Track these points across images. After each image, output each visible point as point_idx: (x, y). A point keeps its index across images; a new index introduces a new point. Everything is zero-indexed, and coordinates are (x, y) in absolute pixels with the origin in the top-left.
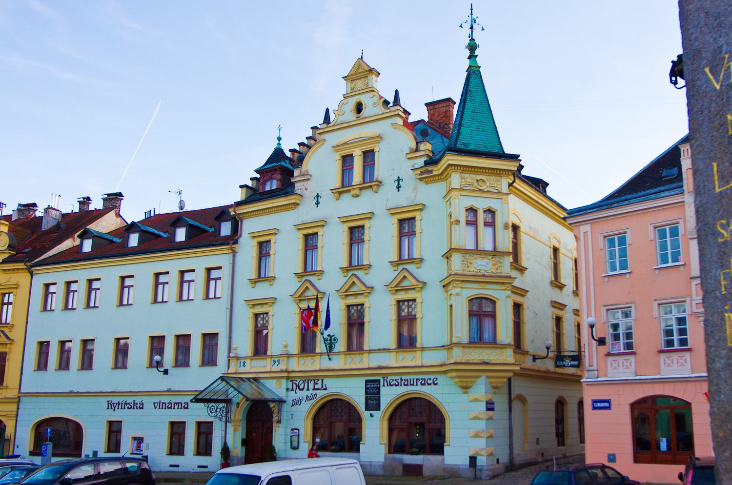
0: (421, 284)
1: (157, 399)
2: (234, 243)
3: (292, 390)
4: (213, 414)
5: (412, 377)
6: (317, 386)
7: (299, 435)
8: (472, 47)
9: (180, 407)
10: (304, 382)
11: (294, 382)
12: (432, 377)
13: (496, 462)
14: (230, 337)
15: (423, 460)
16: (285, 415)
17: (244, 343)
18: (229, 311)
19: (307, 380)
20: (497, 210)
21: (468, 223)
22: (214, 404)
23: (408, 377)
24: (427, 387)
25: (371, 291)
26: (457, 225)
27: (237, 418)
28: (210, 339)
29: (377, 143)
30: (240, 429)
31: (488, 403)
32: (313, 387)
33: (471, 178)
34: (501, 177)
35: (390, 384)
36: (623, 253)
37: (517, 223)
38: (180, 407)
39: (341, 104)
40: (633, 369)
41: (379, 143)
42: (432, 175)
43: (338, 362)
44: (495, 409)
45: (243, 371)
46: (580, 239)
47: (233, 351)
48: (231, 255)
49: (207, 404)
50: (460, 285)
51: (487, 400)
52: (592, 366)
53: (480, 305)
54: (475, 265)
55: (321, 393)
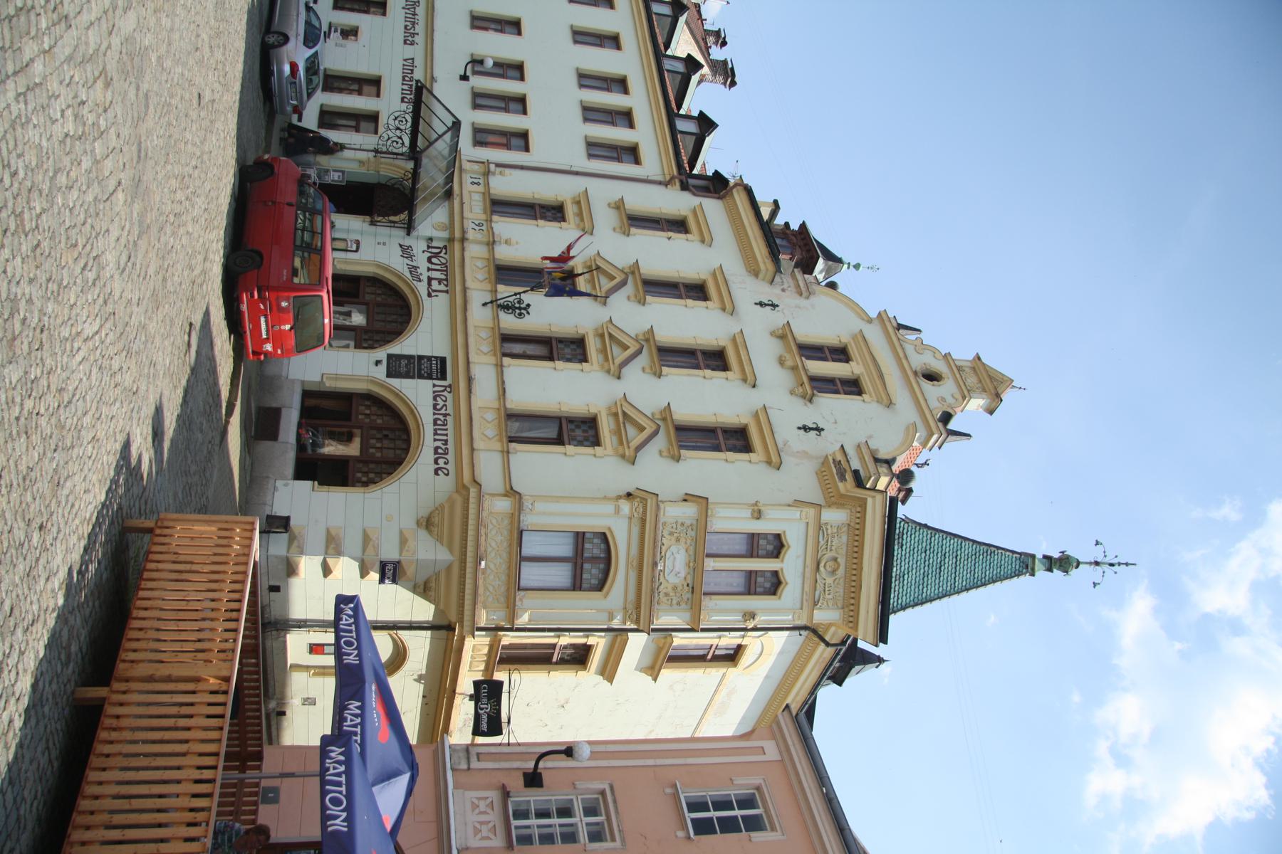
0: (632, 454)
1: (419, 62)
2: (681, 182)
3: (429, 247)
4: (391, 122)
5: (450, 432)
6: (434, 283)
7: (346, 250)
8: (1063, 563)
9: (404, 92)
10: (443, 264)
11: (444, 251)
12: (451, 467)
13: (272, 583)
14: (522, 168)
15: (287, 443)
16: (383, 232)
17: (510, 185)
18: (568, 168)
19: (445, 269)
20: (780, 598)
21: (753, 538)
22: (409, 124)
23: (450, 426)
24: (432, 457)
25: (613, 375)
26: (752, 514)
27: (382, 166)
28: (521, 139)
29: (878, 398)
30: (363, 170)
31: (397, 564)
32: (433, 277)
33: (840, 543)
34: (843, 608)
35: (439, 396)
36: (729, 826)
37: (746, 659)
38: (404, 92)
39: (934, 351)
40: (475, 843)
41: (878, 402)
42: (837, 480)
43: (479, 316)
44: (382, 585)
45: (464, 181)
46: (748, 740)
47: (499, 170)
48: (660, 178)
49: (411, 110)
50: (636, 515)
51: (404, 563)
52: (479, 760)
53: (594, 560)
54: (673, 549)
55: (422, 288)
